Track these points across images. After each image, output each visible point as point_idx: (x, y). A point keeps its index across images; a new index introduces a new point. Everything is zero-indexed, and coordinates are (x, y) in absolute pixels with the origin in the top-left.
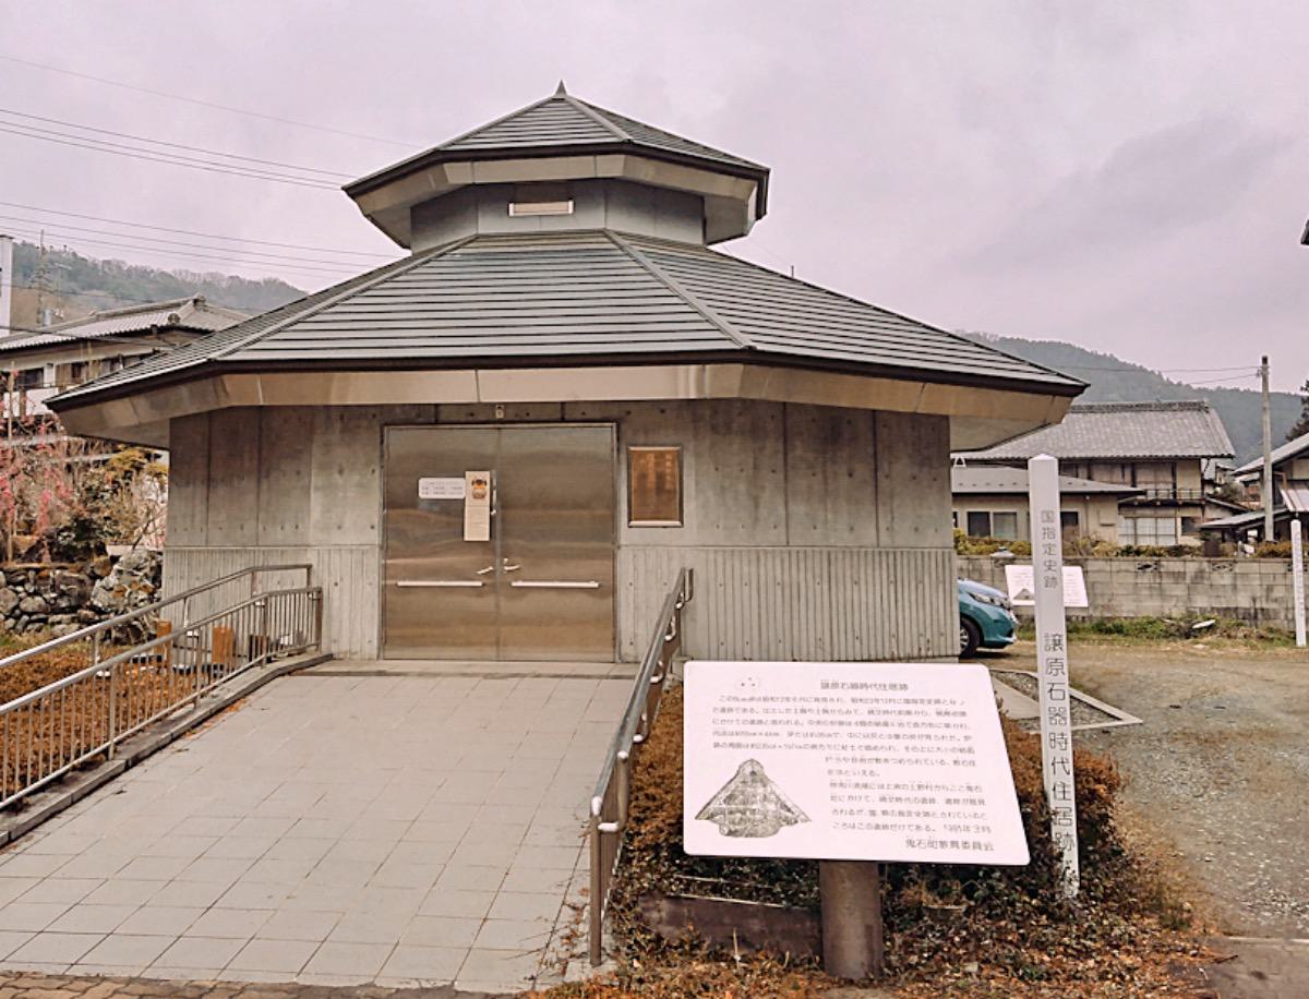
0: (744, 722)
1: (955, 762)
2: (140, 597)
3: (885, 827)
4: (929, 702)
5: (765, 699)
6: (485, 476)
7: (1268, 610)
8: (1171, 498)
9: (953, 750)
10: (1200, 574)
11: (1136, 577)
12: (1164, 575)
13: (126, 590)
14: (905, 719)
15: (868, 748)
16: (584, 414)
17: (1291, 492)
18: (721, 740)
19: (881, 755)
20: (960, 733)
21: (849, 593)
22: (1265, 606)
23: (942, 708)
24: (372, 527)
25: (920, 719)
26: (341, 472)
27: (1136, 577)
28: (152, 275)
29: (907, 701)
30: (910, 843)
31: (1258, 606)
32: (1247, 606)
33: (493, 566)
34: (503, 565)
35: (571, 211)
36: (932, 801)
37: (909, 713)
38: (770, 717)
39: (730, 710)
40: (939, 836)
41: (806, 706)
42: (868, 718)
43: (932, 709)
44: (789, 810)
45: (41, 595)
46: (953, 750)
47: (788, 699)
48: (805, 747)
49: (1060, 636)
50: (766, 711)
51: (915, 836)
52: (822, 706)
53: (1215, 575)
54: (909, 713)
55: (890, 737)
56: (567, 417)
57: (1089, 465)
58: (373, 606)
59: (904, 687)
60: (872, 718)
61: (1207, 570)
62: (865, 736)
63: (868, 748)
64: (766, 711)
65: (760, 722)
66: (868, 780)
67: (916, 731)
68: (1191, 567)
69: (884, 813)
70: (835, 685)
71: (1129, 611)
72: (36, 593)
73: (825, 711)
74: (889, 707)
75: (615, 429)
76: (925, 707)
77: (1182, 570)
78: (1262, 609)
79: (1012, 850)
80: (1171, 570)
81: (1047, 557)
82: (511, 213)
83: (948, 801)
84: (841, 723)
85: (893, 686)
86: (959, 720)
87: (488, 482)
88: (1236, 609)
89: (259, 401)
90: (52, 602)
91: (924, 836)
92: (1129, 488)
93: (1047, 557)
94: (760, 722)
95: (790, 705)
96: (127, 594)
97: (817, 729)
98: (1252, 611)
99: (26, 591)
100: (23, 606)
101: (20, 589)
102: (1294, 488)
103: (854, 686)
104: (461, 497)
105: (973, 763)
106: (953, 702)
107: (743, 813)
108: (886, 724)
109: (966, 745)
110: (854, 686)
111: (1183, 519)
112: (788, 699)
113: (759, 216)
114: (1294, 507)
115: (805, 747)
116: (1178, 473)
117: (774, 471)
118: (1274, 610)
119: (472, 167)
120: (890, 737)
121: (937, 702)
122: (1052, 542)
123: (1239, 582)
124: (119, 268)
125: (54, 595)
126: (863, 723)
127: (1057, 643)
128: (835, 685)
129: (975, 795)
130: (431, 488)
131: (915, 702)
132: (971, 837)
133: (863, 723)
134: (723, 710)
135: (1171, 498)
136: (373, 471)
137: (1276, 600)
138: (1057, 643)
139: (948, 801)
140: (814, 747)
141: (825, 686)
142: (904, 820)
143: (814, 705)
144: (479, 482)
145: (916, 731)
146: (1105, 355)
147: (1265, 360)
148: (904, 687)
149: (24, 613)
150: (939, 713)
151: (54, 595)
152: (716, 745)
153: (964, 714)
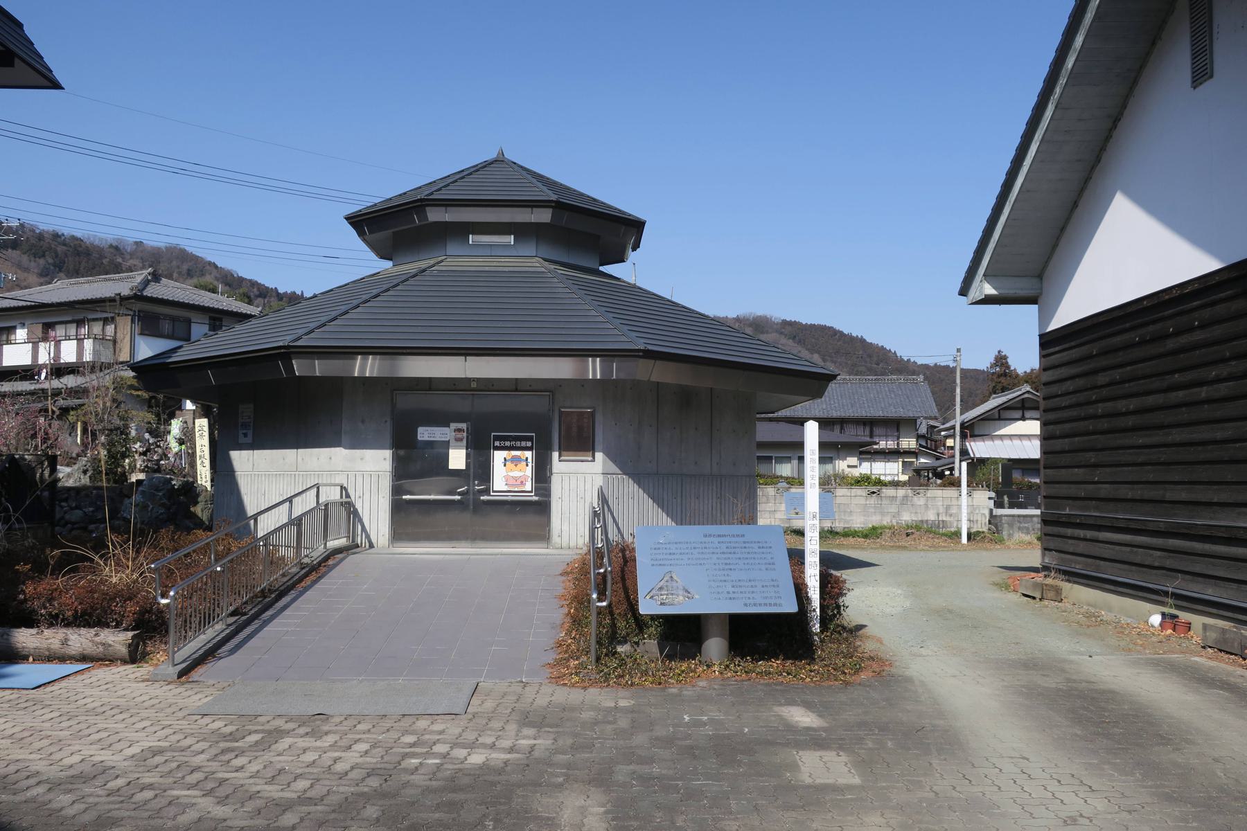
0: (666, 554)
1: (766, 569)
2: (160, 511)
3: (734, 598)
4: (755, 542)
5: (676, 543)
6: (464, 426)
7: (946, 521)
8: (896, 447)
9: (766, 564)
10: (906, 497)
11: (866, 500)
12: (883, 499)
13: (149, 506)
14: (744, 550)
15: (726, 564)
16: (530, 386)
17: (972, 443)
18: (655, 563)
19: (732, 567)
20: (769, 556)
21: (693, 504)
22: (944, 519)
23: (761, 545)
24: (385, 459)
25: (751, 550)
26: (363, 422)
27: (866, 500)
28: (63, 238)
29: (744, 542)
30: (746, 605)
31: (940, 519)
32: (933, 519)
33: (468, 485)
34: (474, 485)
35: (512, 243)
36: (756, 586)
37: (745, 548)
38: (679, 551)
39: (659, 549)
40: (758, 601)
41: (697, 546)
42: (726, 550)
43: (755, 545)
44: (689, 593)
45: (81, 509)
46: (766, 564)
47: (687, 543)
48: (697, 564)
49: (816, 513)
50: (677, 549)
51: (748, 602)
52: (704, 545)
53: (915, 498)
54: (745, 548)
55: (736, 559)
56: (519, 388)
57: (842, 422)
58: (385, 512)
59: (743, 536)
60: (729, 550)
61: (911, 495)
62: (725, 559)
63: (726, 564)
64: (677, 549)
65: (674, 554)
66: (726, 578)
67: (749, 556)
68: (901, 492)
69: (734, 592)
70: (710, 536)
71: (860, 524)
72: (77, 508)
73: (705, 548)
74: (737, 545)
75: (551, 396)
76: (753, 545)
77: (895, 495)
78: (943, 521)
79: (791, 607)
80: (888, 495)
81: (812, 473)
82: (470, 242)
83: (763, 586)
84: (713, 553)
85: (738, 536)
86: (769, 550)
87: (465, 430)
88: (927, 521)
89: (316, 373)
90: (91, 514)
91: (752, 601)
92: (868, 439)
93: (812, 473)
94: (674, 554)
95: (689, 546)
96: (150, 509)
97: (701, 556)
98: (937, 522)
99: (68, 506)
100: (67, 517)
101: (63, 504)
102: (974, 441)
103: (719, 536)
104: (447, 440)
105: (774, 569)
106: (766, 542)
107: (667, 595)
108: (734, 553)
109: (771, 561)
110: (719, 536)
111: (903, 462)
112: (687, 543)
113: (634, 249)
114: (974, 455)
115: (697, 564)
116: (901, 429)
117: (651, 426)
118: (950, 522)
119: (446, 209)
120: (736, 559)
121: (759, 542)
122: (814, 465)
123: (930, 503)
124: (34, 231)
125: (91, 509)
126: (723, 553)
127: (814, 517)
128: (710, 536)
129: (775, 583)
130: (425, 434)
131: (748, 542)
132: (773, 602)
133: (723, 553)
134: (655, 549)
135: (896, 447)
136: (386, 422)
137: (951, 515)
138: (814, 517)
139: (763, 586)
140: (701, 564)
141: (705, 536)
142: (741, 595)
143: (700, 546)
144: (459, 430)
145: (749, 556)
146: (857, 336)
147: (959, 350)
148: (743, 536)
149: (67, 523)
150: (759, 548)
151: (91, 509)
152: (653, 565)
153: (770, 547)
